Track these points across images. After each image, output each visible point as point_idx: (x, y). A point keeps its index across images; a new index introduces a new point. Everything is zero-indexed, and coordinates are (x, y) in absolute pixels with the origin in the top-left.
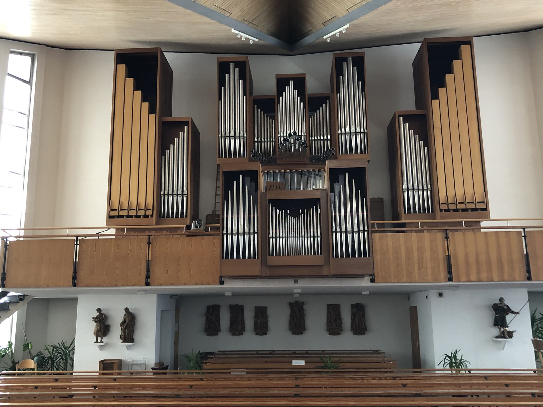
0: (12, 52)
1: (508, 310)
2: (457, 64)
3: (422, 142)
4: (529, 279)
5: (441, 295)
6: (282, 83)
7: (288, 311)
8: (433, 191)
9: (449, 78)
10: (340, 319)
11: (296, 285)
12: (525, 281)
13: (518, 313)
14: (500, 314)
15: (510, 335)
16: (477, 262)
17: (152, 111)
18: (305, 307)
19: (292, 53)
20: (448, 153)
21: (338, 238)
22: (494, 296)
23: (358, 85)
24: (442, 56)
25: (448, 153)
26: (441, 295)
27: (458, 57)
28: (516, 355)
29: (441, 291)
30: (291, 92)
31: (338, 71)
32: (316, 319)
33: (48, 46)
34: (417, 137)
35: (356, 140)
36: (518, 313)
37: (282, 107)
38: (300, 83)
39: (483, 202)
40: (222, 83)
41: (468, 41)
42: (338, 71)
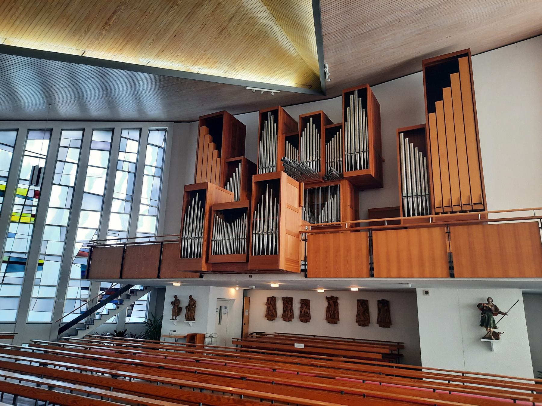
0: (151, 130)
1: (497, 312)
2: (454, 77)
3: (421, 153)
4: (452, 276)
5: (427, 293)
6: (305, 120)
7: (326, 304)
8: (430, 196)
9: (446, 91)
10: (368, 313)
11: (251, 279)
12: (448, 277)
13: (506, 314)
14: (487, 314)
15: (497, 336)
16: (399, 261)
17: (219, 156)
18: (338, 301)
19: (325, 97)
20: (444, 160)
21: (256, 239)
22: (482, 295)
23: (362, 112)
24: (442, 71)
25: (444, 160)
26: (427, 293)
27: (456, 70)
28: (509, 358)
29: (426, 289)
30: (311, 126)
31: (347, 104)
32: (347, 311)
33: (175, 122)
34: (416, 149)
35: (360, 158)
36: (506, 314)
37: (303, 141)
38: (317, 118)
39: (481, 203)
40: (262, 128)
41: (466, 54)
42: (347, 104)
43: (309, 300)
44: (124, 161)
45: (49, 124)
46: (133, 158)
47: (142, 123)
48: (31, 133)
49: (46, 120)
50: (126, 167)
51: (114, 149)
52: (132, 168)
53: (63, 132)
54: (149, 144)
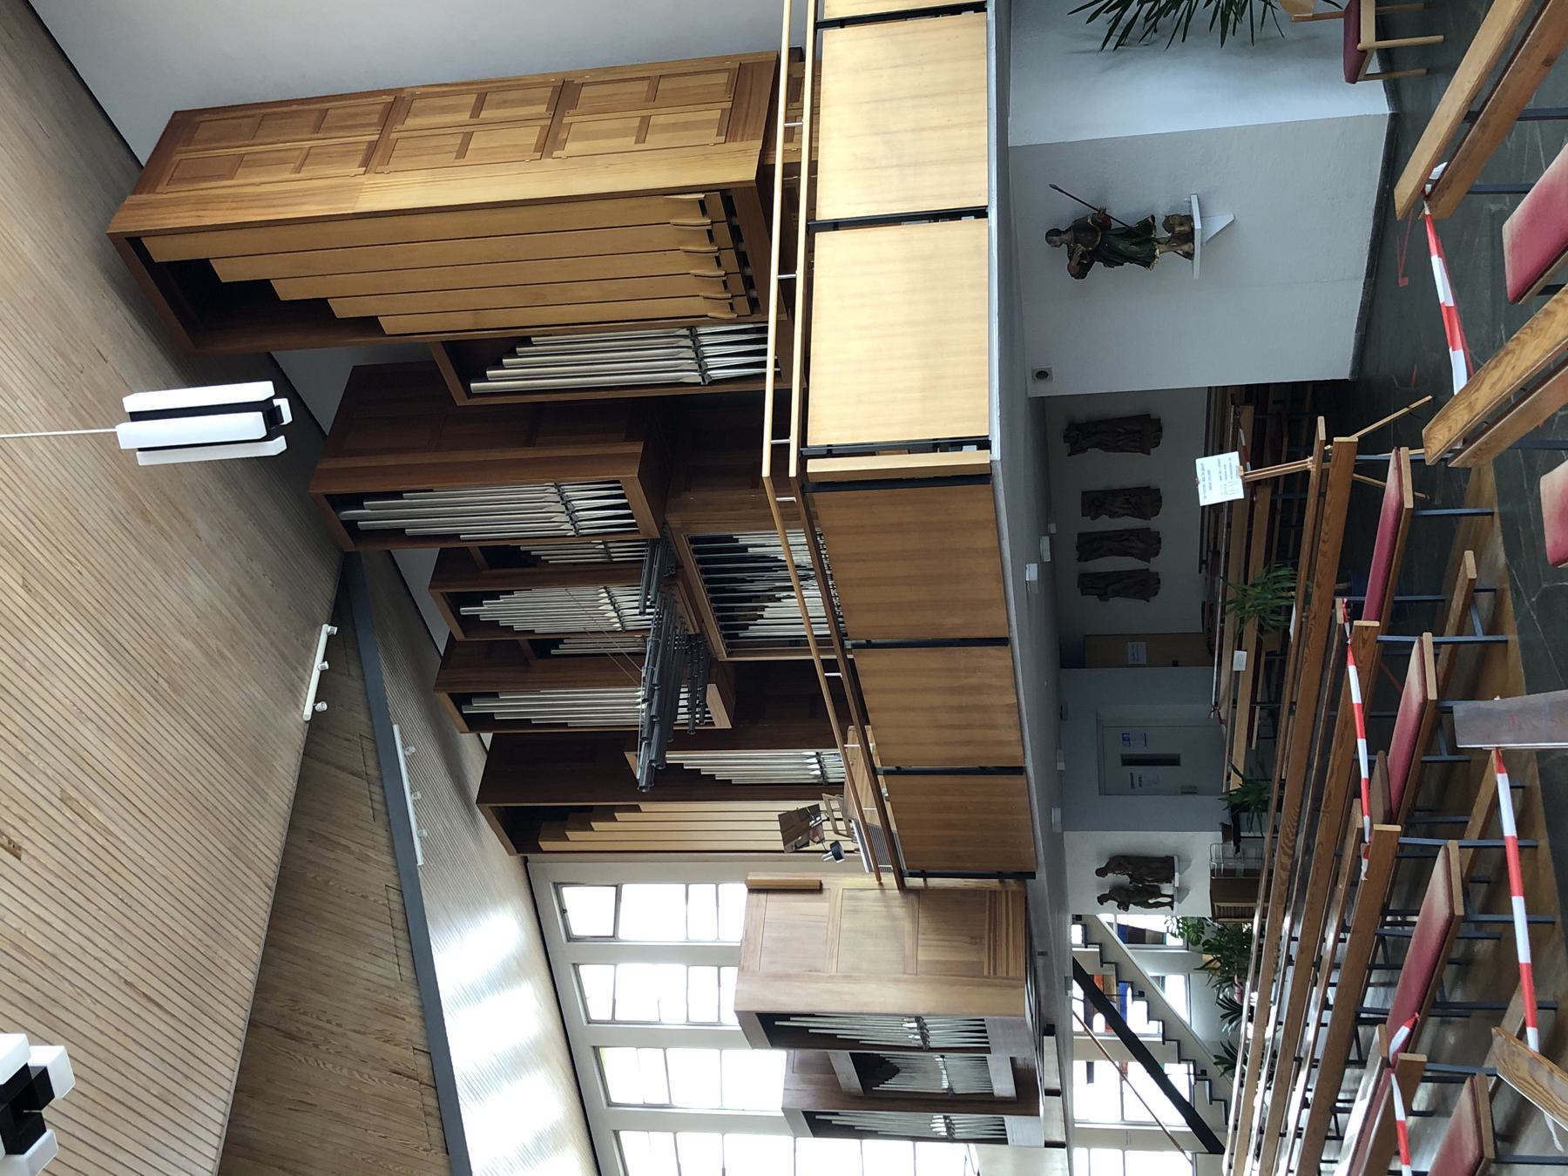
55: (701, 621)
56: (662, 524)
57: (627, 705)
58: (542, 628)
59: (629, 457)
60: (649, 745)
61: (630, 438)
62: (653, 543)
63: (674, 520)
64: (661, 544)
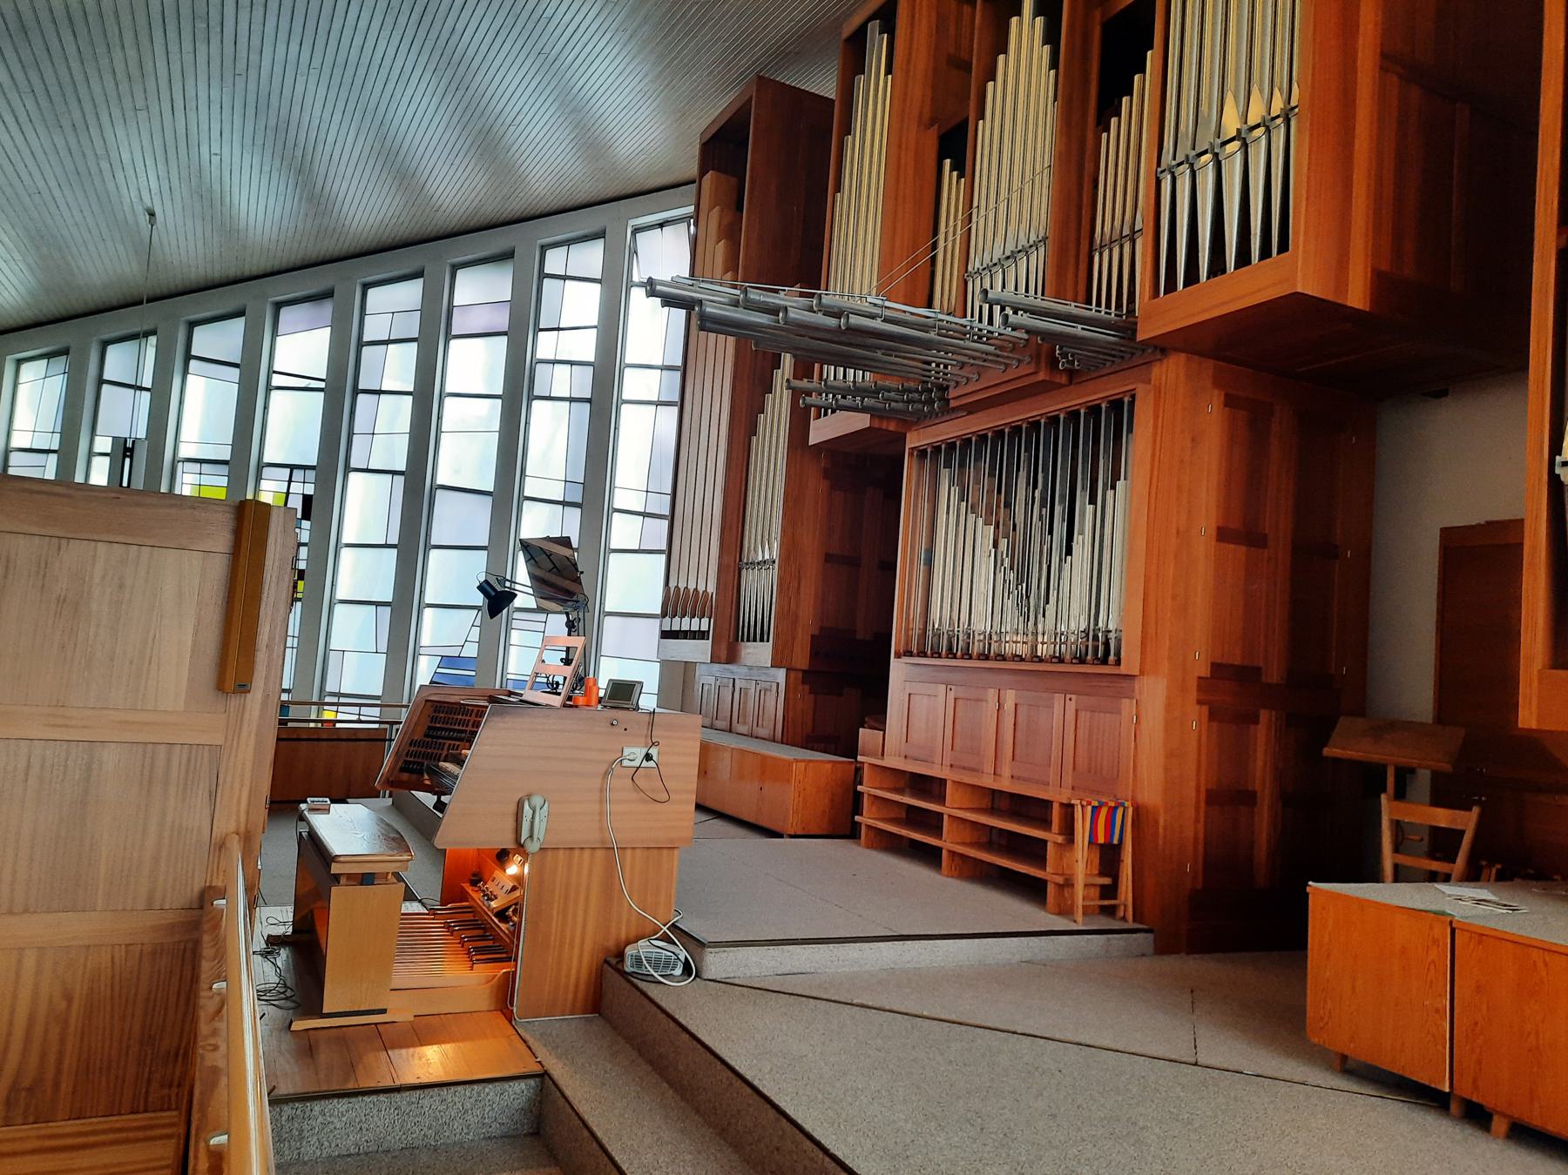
43: (1444, 531)
44: (554, 362)
45: (326, 272)
46: (584, 346)
47: (601, 208)
48: (286, 314)
49: (140, 303)
50: (561, 381)
51: (522, 325)
52: (582, 383)
53: (372, 292)
54: (504, 333)
55: (971, 409)
56: (1162, 347)
57: (857, 277)
58: (985, 132)
59: (1341, 282)
60: (736, 304)
61: (1381, 282)
62: (1127, 329)
63: (1171, 371)
64: (1130, 348)
